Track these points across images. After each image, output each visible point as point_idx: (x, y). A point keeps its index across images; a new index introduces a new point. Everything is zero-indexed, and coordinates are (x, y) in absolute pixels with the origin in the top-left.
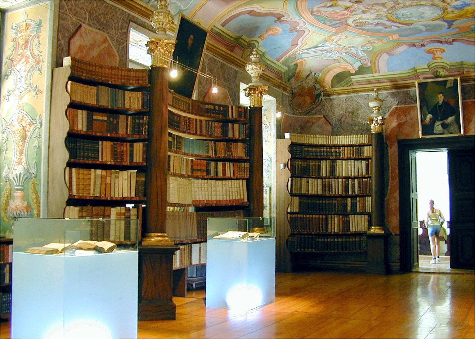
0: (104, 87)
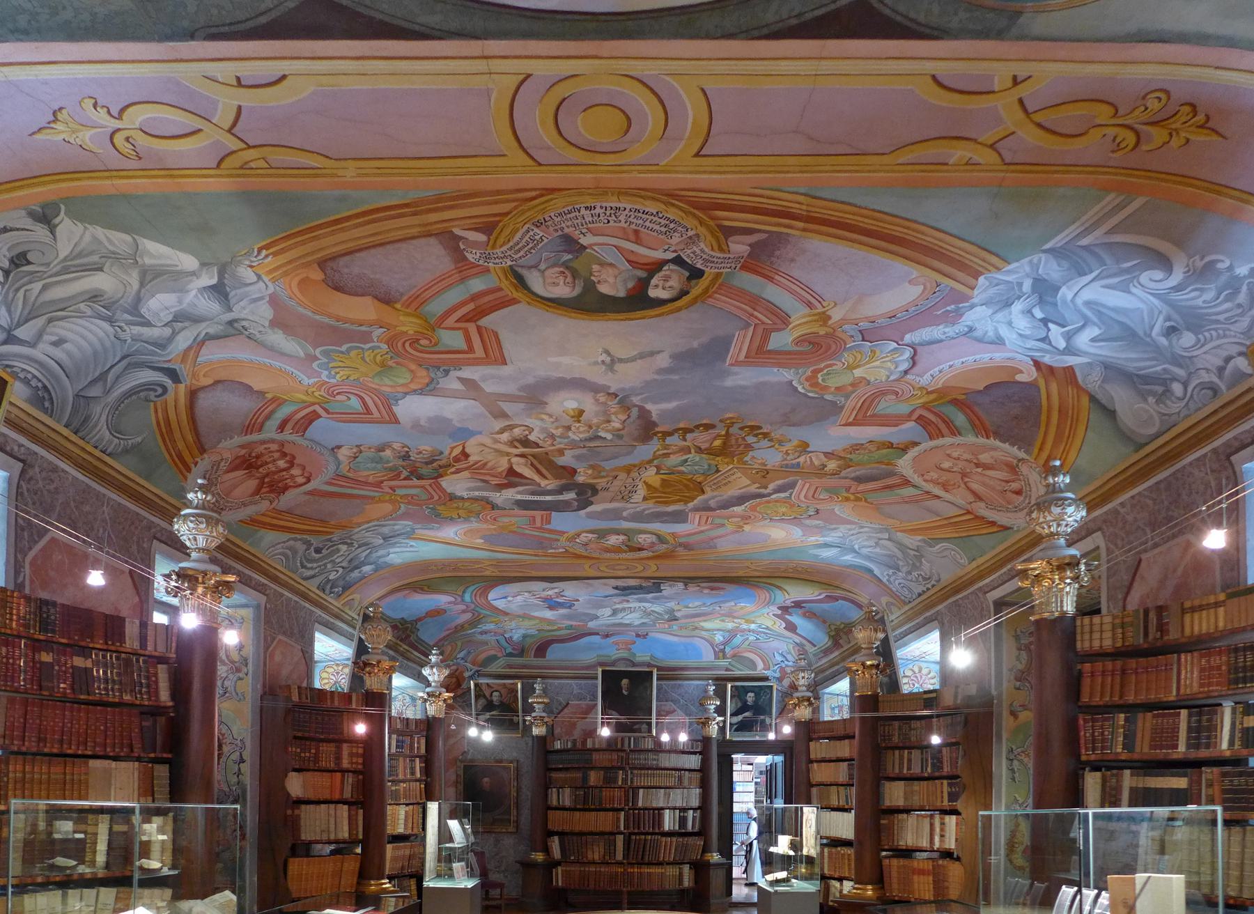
0: (736, 797)
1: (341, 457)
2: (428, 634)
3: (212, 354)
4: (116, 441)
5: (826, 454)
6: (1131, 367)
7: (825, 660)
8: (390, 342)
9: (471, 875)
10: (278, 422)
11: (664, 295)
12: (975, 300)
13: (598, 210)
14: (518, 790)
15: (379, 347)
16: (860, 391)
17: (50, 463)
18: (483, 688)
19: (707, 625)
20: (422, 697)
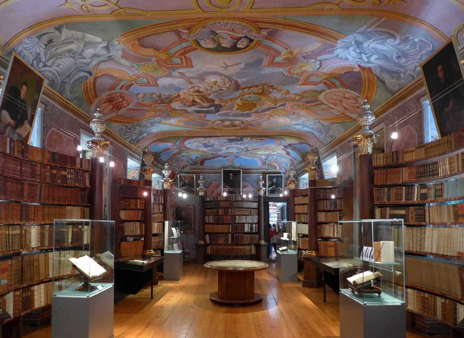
0: (270, 219)
1: (139, 97)
2: (164, 157)
3: (103, 66)
4: (72, 95)
5: (295, 94)
6: (388, 68)
7: (300, 166)
8: (158, 61)
9: (179, 249)
10: (120, 87)
11: (242, 47)
12: (338, 47)
13: (221, 24)
14: (195, 216)
15: (154, 63)
16: (304, 74)
17: (53, 104)
18: (182, 177)
19: (259, 153)
20: (162, 182)
